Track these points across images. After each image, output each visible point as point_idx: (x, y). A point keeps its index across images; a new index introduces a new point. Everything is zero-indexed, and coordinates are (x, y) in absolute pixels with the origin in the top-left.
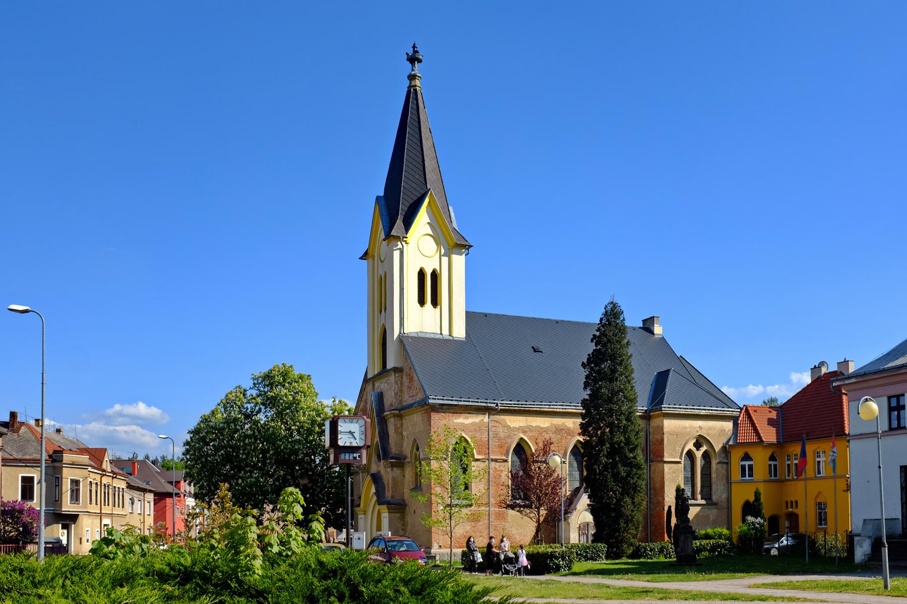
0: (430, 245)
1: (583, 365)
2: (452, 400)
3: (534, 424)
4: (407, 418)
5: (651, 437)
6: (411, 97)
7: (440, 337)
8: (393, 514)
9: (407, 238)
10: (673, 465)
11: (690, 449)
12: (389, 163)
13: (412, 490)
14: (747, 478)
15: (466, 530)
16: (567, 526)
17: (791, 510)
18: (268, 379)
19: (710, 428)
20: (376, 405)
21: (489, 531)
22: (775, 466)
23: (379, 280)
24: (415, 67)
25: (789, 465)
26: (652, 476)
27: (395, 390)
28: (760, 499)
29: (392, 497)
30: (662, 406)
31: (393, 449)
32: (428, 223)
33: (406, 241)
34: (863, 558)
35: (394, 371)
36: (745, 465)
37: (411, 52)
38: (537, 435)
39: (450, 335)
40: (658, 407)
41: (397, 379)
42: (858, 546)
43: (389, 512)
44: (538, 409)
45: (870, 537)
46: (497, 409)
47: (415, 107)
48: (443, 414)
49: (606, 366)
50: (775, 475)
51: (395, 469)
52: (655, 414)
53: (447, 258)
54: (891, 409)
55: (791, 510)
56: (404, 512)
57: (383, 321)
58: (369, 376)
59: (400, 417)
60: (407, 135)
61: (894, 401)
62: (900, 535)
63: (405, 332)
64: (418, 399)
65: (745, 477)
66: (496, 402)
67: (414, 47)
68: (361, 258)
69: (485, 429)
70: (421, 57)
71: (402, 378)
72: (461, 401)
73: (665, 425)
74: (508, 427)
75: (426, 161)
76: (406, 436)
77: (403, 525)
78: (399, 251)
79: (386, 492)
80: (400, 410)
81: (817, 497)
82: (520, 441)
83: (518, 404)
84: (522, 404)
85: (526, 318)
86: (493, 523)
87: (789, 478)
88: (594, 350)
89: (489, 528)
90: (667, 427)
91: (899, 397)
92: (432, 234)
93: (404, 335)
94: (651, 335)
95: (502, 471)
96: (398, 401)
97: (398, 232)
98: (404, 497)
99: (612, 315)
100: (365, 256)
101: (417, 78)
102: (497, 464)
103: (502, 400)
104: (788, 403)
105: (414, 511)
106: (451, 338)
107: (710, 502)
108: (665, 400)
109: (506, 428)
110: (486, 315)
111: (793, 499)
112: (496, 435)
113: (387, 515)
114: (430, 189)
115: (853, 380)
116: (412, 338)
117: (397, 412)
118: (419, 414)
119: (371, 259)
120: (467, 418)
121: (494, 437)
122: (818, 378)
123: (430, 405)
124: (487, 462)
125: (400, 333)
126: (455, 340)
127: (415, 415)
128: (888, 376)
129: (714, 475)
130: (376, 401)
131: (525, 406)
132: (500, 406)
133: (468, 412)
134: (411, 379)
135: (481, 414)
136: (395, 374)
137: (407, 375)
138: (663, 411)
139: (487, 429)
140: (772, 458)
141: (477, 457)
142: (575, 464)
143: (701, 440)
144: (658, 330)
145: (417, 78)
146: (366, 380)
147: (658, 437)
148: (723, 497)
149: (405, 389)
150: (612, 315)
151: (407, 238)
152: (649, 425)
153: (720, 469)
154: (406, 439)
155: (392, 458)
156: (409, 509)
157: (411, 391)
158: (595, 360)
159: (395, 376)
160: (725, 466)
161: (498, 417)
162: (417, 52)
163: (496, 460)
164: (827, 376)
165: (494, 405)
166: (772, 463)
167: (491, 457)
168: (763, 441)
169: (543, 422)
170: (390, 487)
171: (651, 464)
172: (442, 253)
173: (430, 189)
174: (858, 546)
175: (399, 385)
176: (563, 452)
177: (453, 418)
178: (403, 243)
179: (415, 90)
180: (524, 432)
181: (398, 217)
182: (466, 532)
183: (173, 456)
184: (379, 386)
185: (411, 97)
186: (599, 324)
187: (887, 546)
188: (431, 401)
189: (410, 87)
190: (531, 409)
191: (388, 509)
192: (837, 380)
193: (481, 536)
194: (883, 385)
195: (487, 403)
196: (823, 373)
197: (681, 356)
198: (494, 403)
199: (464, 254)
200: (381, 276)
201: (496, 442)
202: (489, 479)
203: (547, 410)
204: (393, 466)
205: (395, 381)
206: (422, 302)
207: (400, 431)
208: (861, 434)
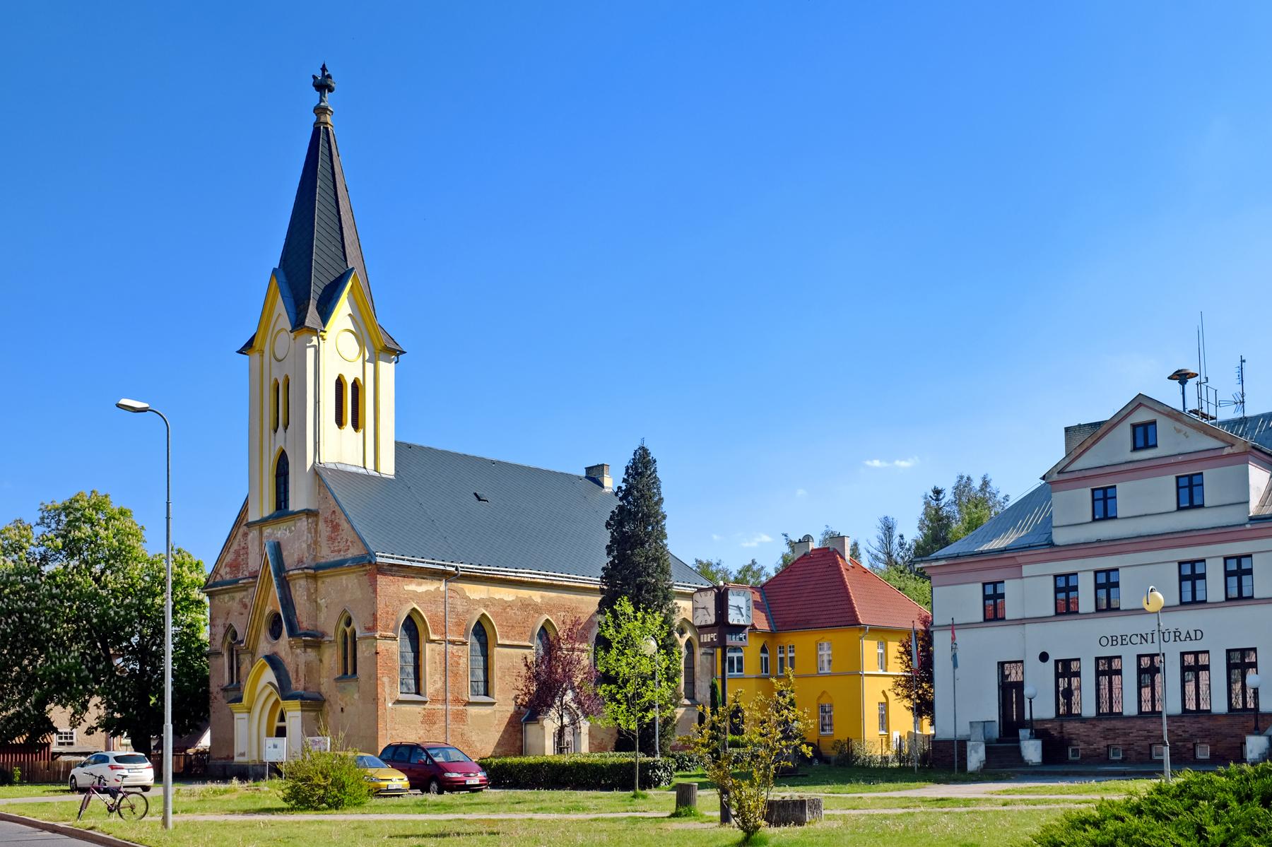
0: (350, 345)
2: (404, 560)
3: (497, 597)
4: (328, 580)
7: (362, 471)
8: (307, 713)
9: (325, 332)
13: (337, 680)
14: (736, 673)
16: (540, 731)
18: (70, 514)
20: (274, 560)
21: (446, 737)
22: (766, 659)
24: (325, 97)
25: (781, 659)
27: (307, 540)
31: (304, 622)
32: (350, 315)
33: (322, 336)
34: (979, 765)
35: (307, 514)
36: (733, 657)
37: (319, 74)
39: (376, 470)
41: (310, 525)
43: (302, 711)
44: (503, 577)
46: (456, 575)
47: (327, 152)
48: (391, 578)
50: (766, 672)
51: (309, 650)
53: (372, 365)
56: (321, 710)
58: (253, 516)
59: (315, 578)
62: (997, 739)
66: (455, 564)
67: (324, 69)
68: (240, 352)
70: (333, 85)
71: (317, 525)
72: (414, 561)
74: (468, 599)
75: (344, 229)
78: (313, 349)
81: (819, 698)
82: (411, 613)
83: (481, 569)
84: (485, 570)
87: (782, 674)
92: (354, 330)
93: (320, 465)
95: (460, 656)
96: (311, 557)
98: (320, 689)
100: (248, 347)
101: (328, 112)
102: (455, 647)
104: (772, 583)
105: (342, 709)
106: (377, 474)
107: (694, 703)
112: (453, 609)
114: (353, 268)
115: (943, 562)
117: (312, 571)
118: (353, 576)
119: (256, 356)
120: (420, 584)
122: (805, 554)
123: (377, 565)
125: (315, 462)
127: (344, 577)
129: (697, 669)
130: (272, 554)
132: (461, 571)
133: (421, 576)
134: (335, 527)
135: (437, 580)
136: (308, 518)
139: (444, 600)
140: (764, 650)
141: (433, 637)
142: (478, 647)
143: (686, 625)
145: (328, 112)
149: (323, 540)
151: (325, 332)
153: (705, 661)
154: (324, 610)
156: (330, 705)
158: (619, 520)
160: (709, 657)
161: (455, 584)
162: (329, 77)
163: (453, 643)
164: (816, 552)
165: (454, 569)
166: (764, 655)
167: (448, 638)
168: (756, 629)
170: (301, 675)
172: (367, 358)
173: (353, 268)
175: (313, 535)
176: (529, 634)
177: (403, 583)
179: (327, 129)
180: (486, 606)
181: (309, 302)
182: (420, 738)
188: (379, 560)
190: (508, 577)
192: (922, 561)
194: (976, 570)
195: (444, 565)
196: (810, 549)
199: (394, 362)
200: (276, 380)
202: (446, 667)
203: (513, 578)
204: (307, 645)
205: (308, 529)
206: (340, 422)
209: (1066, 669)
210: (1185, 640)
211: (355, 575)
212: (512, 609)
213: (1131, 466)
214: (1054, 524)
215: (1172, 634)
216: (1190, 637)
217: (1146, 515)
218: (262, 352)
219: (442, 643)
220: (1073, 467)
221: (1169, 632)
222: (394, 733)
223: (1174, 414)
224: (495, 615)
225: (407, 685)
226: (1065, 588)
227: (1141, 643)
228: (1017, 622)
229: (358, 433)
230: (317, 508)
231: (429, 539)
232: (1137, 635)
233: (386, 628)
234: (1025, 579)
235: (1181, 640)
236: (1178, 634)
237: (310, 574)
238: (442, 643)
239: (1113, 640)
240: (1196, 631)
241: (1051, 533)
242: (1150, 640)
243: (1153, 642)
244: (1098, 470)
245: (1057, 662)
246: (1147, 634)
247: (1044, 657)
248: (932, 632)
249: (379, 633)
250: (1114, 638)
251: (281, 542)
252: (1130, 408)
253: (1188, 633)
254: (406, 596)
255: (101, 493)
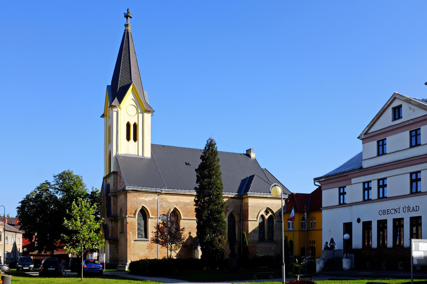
1: (196, 170)
3: (182, 201)
4: (119, 197)
5: (243, 208)
6: (126, 36)
9: (120, 106)
10: (253, 222)
11: (262, 214)
12: (114, 69)
15: (145, 253)
17: (312, 245)
18: (61, 176)
19: (273, 204)
21: (158, 254)
23: (109, 127)
24: (128, 20)
25: (311, 223)
26: (243, 227)
28: (288, 239)
29: (111, 237)
30: (248, 193)
34: (320, 270)
37: (126, 12)
38: (183, 206)
40: (246, 193)
42: (317, 263)
43: (109, 244)
45: (323, 259)
49: (206, 172)
51: (113, 222)
52: (245, 197)
54: (340, 194)
55: (312, 245)
56: (118, 244)
57: (110, 149)
60: (123, 54)
61: (342, 189)
63: (119, 154)
64: (123, 187)
65: (290, 229)
67: (128, 10)
69: (156, 202)
71: (117, 177)
73: (249, 202)
74: (168, 202)
76: (118, 206)
77: (117, 250)
79: (109, 233)
80: (115, 193)
85: (189, 148)
86: (160, 250)
88: (201, 163)
89: (158, 252)
90: (250, 203)
91: (344, 187)
93: (118, 155)
94: (249, 157)
97: (115, 103)
98: (117, 236)
99: (211, 145)
100: (103, 116)
103: (165, 189)
106: (143, 157)
108: (250, 190)
109: (167, 203)
110: (164, 146)
111: (313, 240)
112: (162, 206)
113: (108, 245)
115: (323, 179)
116: (122, 157)
120: (146, 197)
121: (160, 207)
124: (157, 219)
125: (116, 154)
126: (145, 158)
127: (122, 195)
128: (340, 177)
130: (105, 188)
131: (177, 192)
134: (120, 177)
137: (119, 175)
138: (248, 195)
139: (157, 203)
144: (253, 155)
146: (104, 178)
147: (246, 208)
148: (279, 238)
150: (211, 145)
151: (120, 106)
152: (242, 202)
155: (112, 217)
157: (120, 184)
159: (113, 176)
169: (187, 200)
170: (111, 231)
171: (243, 221)
172: (139, 112)
174: (317, 263)
178: (118, 109)
179: (128, 32)
180: (177, 205)
183: (4, 214)
184: (108, 181)
185: (126, 36)
186: (204, 150)
187: (285, 264)
189: (125, 30)
191: (109, 243)
193: (153, 256)
197: (265, 169)
198: (161, 190)
201: (162, 209)
205: (113, 179)
206: (128, 139)
207: (116, 203)
208: (327, 207)
209: (367, 226)
210: (412, 211)
211: (123, 195)
212: (189, 205)
213: (391, 128)
214: (363, 159)
215: (407, 208)
216: (414, 210)
217: (397, 151)
218: (107, 116)
219: (128, 217)
220: (370, 131)
221: (406, 208)
222: (134, 252)
223: (408, 100)
224: (181, 208)
225: (141, 235)
226: (367, 188)
227: (395, 213)
228: (349, 205)
229: (136, 143)
230: (117, 171)
231: (236, 179)
232: (393, 209)
233: (131, 213)
234: (353, 185)
235: (410, 211)
236: (409, 208)
237: (114, 195)
238: (128, 217)
239: (385, 212)
240: (416, 206)
241: (362, 162)
242: (398, 212)
243: (399, 213)
244: (378, 131)
245: (364, 223)
246: (397, 209)
247: (359, 221)
248: (322, 210)
249: (128, 216)
250: (385, 211)
251: (110, 184)
252: (391, 100)
253: (413, 208)
254: (140, 202)
255: (71, 171)
